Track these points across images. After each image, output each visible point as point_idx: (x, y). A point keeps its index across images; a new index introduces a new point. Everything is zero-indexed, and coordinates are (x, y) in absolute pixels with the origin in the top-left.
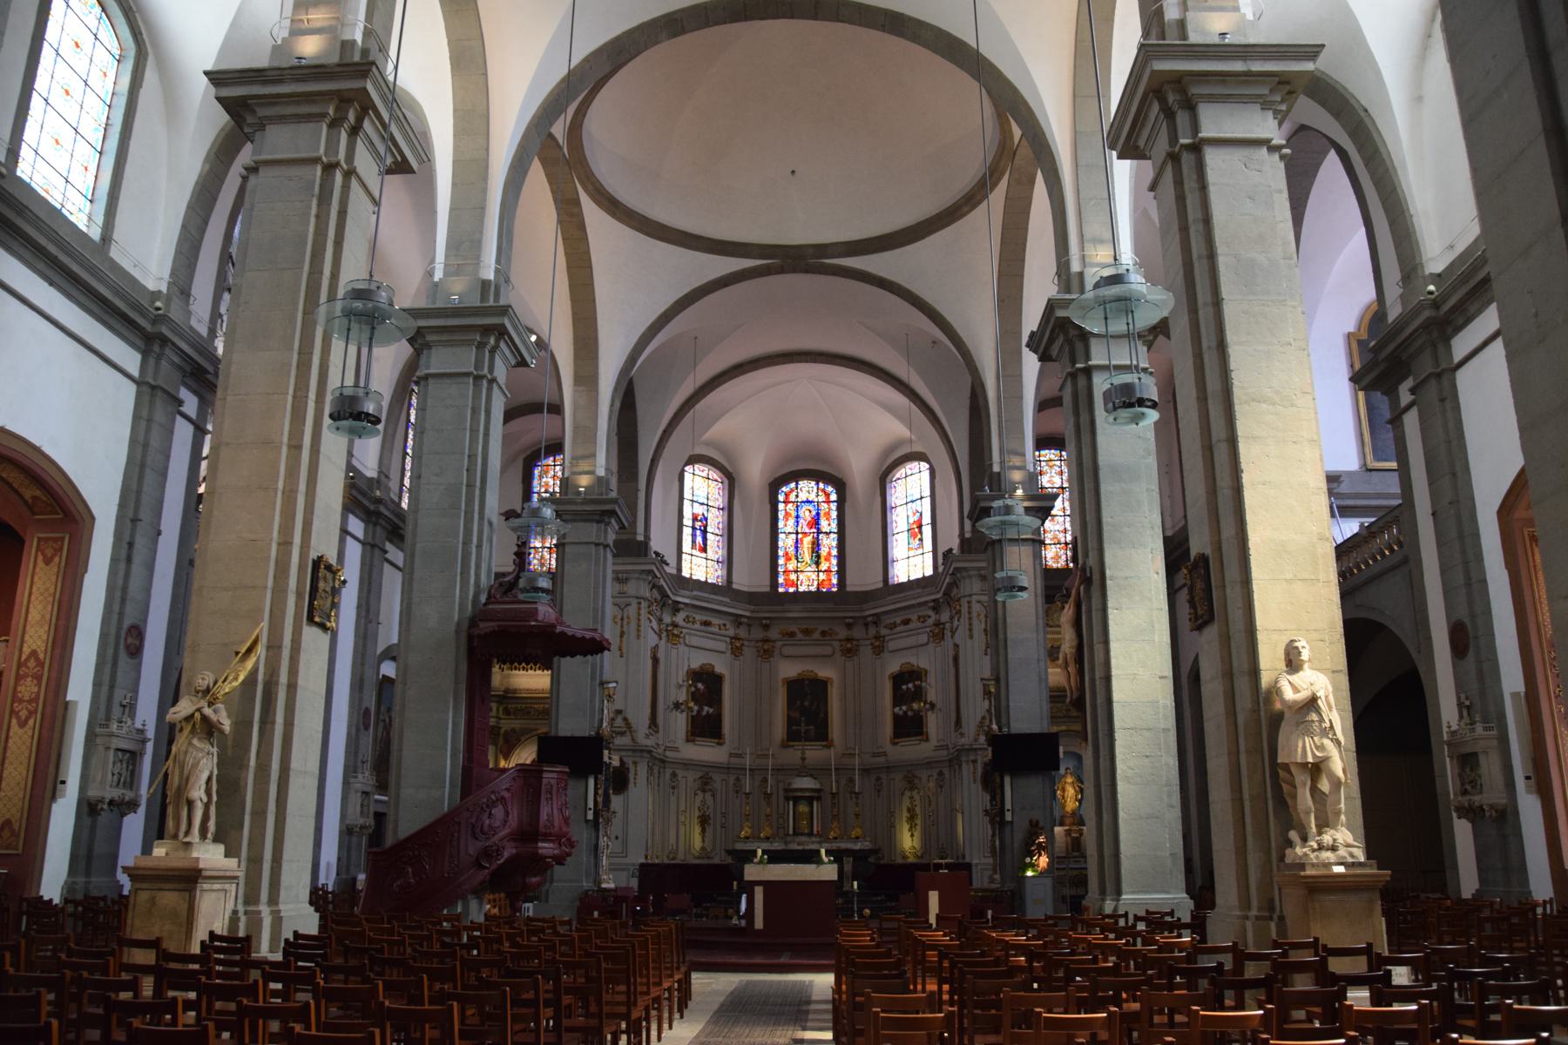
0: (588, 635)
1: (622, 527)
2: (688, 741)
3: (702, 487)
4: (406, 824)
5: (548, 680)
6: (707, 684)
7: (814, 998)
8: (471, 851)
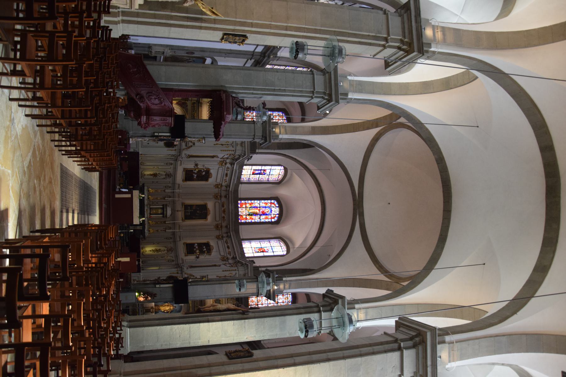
0: (221, 133)
1: (261, 144)
2: (184, 169)
3: (276, 172)
6: (205, 175)
7: (90, 217)
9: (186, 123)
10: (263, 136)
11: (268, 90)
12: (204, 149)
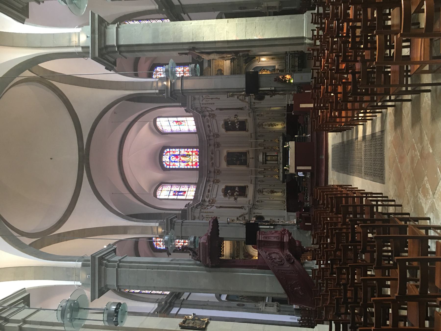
0: (211, 224)
1: (176, 217)
3: (165, 193)
4: (278, 290)
5: (227, 241)
6: (229, 191)
7: (341, 141)
8: (288, 266)
9: (245, 237)
10: (174, 225)
11: (164, 268)
12: (230, 215)
